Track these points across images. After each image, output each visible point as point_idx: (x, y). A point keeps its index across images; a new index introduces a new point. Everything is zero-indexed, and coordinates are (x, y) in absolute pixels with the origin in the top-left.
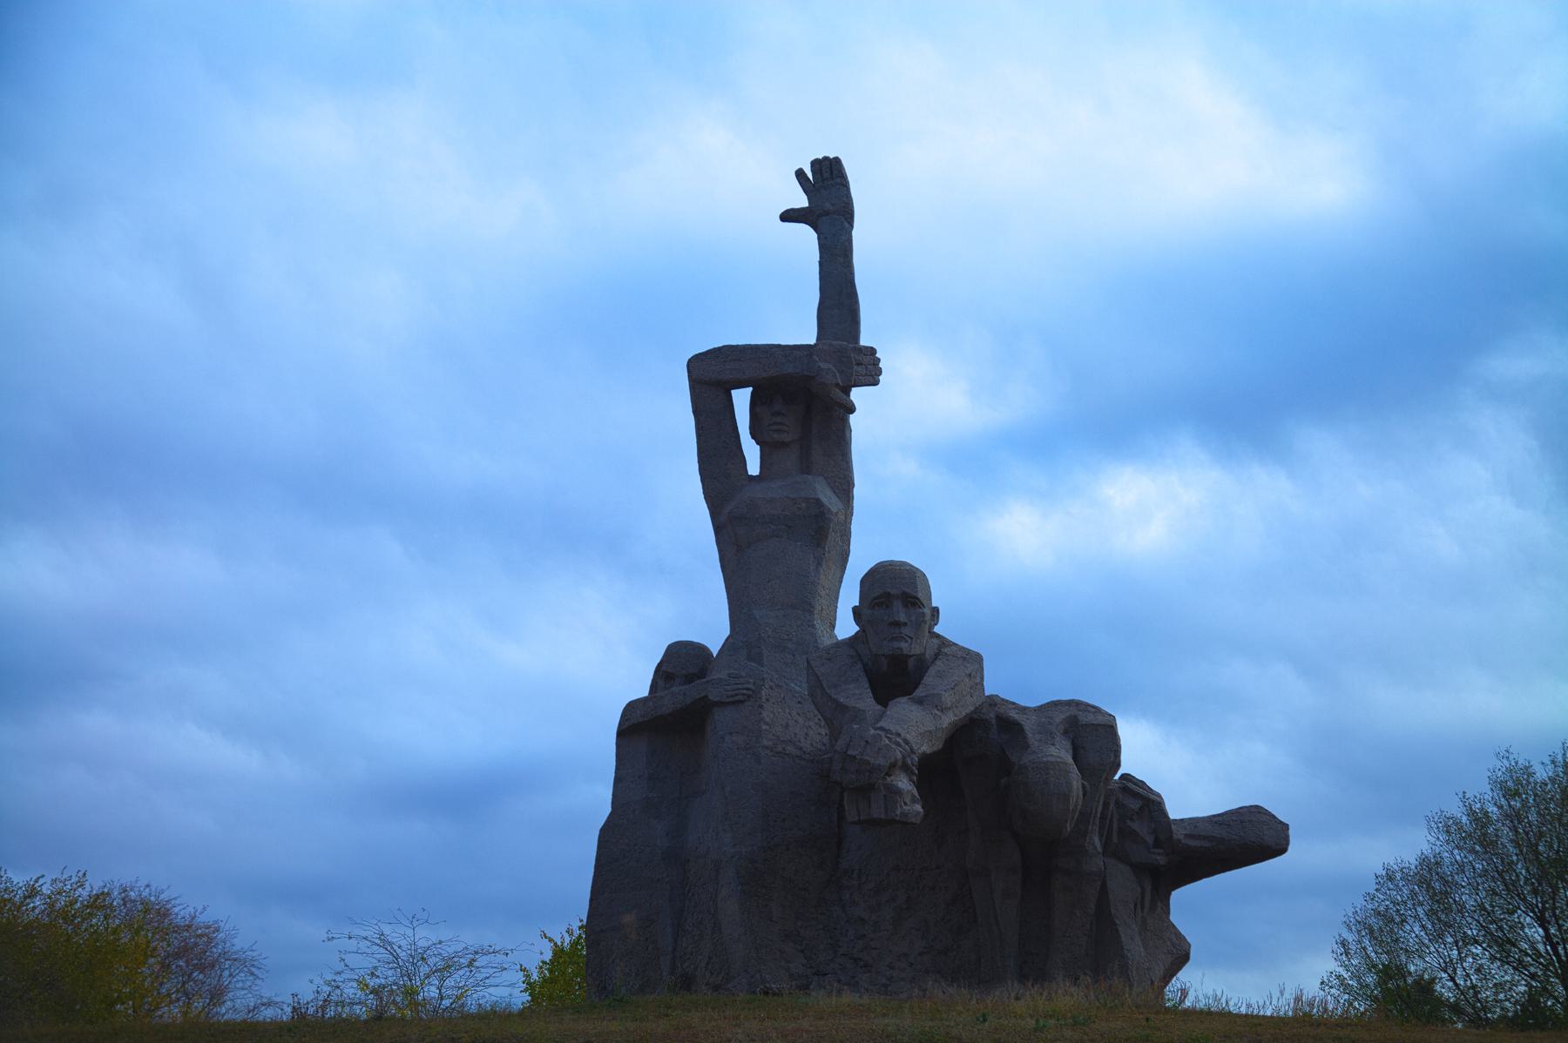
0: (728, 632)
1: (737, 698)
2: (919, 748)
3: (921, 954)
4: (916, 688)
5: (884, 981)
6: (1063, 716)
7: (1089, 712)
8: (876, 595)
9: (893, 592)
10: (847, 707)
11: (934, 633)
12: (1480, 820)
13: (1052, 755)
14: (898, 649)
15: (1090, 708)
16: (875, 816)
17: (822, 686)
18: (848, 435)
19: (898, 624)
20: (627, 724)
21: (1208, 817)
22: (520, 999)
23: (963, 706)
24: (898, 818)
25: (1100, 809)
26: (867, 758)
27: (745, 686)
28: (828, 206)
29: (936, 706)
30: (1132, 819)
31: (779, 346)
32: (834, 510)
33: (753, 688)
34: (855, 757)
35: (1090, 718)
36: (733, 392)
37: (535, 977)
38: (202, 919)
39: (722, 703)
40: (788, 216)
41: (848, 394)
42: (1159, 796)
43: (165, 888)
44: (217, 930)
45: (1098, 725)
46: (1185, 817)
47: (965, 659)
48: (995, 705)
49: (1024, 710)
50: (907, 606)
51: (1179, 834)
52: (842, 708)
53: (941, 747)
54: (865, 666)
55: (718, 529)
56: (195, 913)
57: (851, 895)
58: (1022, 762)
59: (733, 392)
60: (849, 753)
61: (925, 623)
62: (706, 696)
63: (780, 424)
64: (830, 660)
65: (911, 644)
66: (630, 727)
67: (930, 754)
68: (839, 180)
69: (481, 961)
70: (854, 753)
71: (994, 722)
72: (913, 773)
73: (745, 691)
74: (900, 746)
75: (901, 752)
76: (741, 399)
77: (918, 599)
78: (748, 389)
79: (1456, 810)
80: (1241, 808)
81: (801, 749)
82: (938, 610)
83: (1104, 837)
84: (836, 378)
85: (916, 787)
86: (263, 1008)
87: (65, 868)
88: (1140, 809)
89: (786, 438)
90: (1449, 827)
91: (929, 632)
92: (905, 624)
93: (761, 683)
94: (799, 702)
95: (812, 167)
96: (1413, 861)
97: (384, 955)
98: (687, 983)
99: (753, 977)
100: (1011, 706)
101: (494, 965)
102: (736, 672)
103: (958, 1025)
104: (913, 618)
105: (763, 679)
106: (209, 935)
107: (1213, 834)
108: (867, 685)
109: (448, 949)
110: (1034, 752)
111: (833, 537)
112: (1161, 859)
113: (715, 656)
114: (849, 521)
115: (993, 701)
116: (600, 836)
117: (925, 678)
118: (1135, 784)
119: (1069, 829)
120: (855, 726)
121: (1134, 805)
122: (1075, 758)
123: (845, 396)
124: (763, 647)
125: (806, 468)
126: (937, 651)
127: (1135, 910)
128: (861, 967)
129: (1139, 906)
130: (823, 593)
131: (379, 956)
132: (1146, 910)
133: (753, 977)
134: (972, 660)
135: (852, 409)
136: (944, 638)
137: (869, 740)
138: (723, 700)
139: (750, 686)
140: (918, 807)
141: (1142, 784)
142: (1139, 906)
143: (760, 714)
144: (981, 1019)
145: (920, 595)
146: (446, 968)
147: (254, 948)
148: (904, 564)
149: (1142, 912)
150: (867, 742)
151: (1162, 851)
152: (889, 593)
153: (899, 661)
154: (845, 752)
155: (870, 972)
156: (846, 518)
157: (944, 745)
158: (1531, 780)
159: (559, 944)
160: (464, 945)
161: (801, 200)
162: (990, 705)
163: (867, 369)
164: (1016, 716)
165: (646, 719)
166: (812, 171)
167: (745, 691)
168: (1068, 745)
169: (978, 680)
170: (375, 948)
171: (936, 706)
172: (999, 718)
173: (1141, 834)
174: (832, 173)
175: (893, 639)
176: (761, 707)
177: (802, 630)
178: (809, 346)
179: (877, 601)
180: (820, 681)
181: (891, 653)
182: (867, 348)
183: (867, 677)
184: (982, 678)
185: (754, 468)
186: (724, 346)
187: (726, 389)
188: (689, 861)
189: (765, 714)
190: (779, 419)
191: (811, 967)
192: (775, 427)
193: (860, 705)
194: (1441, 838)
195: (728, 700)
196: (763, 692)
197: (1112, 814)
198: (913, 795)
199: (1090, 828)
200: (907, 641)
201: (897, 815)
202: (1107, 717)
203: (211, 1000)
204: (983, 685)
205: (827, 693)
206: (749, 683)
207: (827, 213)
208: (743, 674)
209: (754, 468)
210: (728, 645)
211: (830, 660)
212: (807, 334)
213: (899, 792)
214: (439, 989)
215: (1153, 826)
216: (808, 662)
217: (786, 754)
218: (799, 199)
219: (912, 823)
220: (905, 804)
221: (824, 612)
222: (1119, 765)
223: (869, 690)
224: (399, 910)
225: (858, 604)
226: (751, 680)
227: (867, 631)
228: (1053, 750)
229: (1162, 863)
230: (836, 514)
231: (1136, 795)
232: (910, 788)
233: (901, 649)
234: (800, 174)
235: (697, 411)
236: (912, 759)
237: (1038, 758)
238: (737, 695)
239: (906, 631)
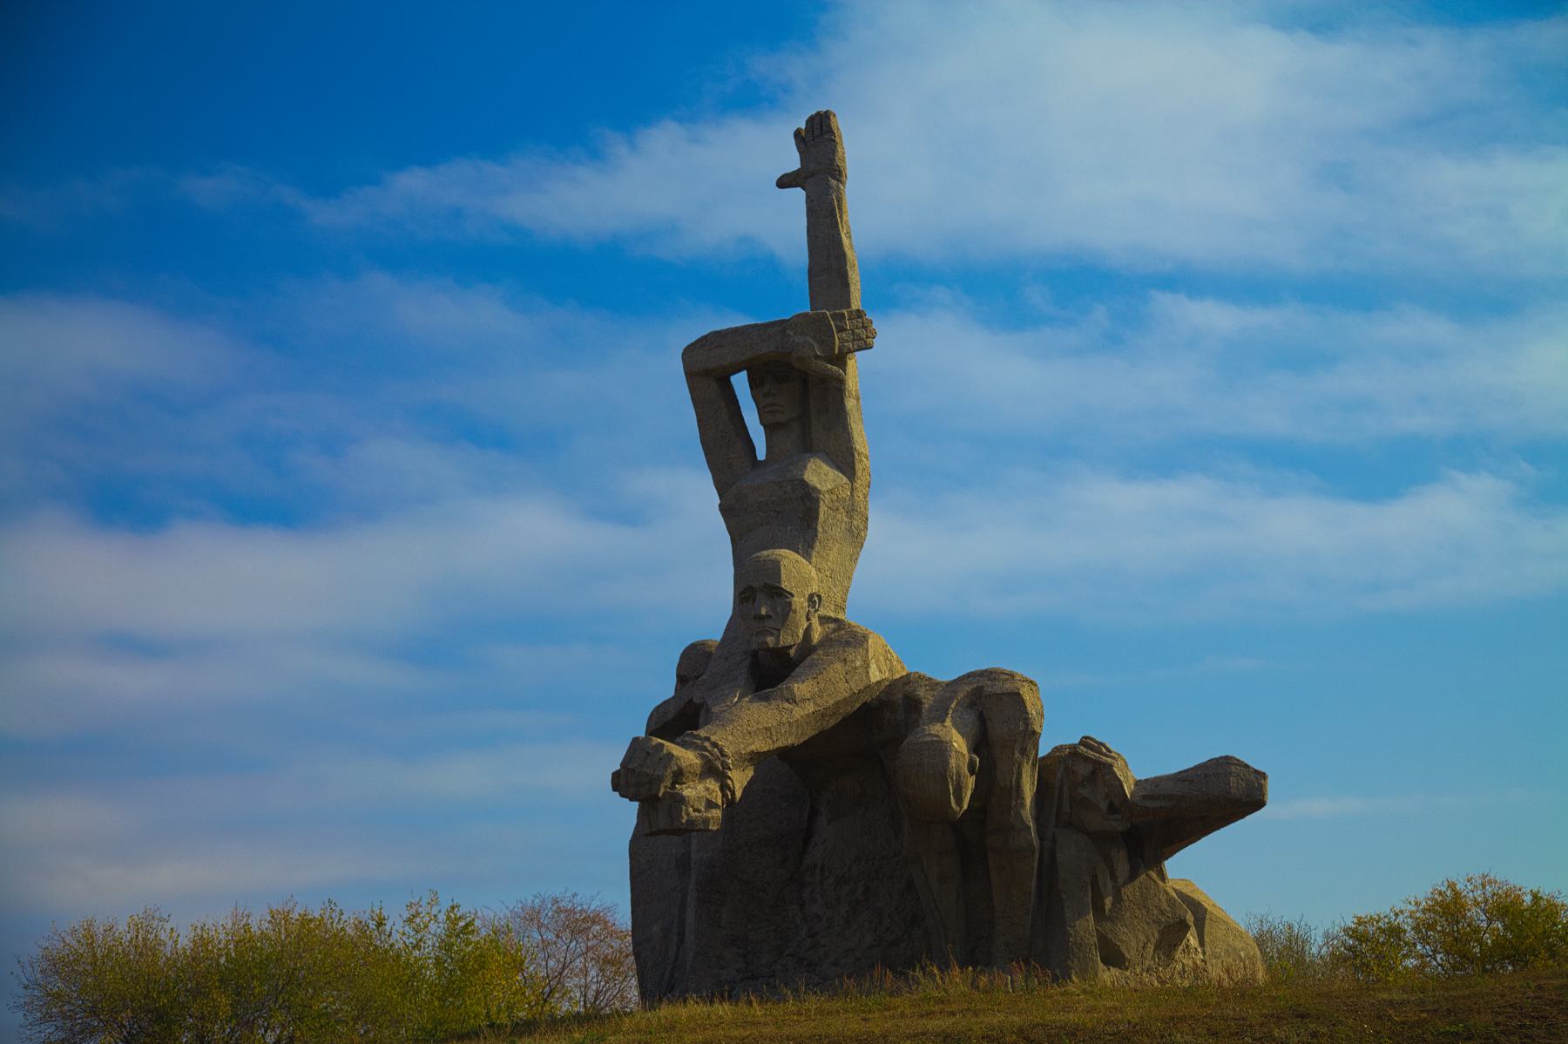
19: (760, 618)
40: (785, 182)
43: (436, 913)
45: (1003, 694)
50: (773, 597)
60: (629, 767)
63: (774, 405)
65: (779, 636)
76: (740, 382)
77: (782, 589)
78: (742, 373)
84: (814, 351)
87: (412, 893)
92: (768, 616)
96: (184, 942)
121: (1083, 770)
125: (808, 448)
137: (651, 751)
151: (1120, 817)
156: (852, 492)
190: (770, 400)
199: (1014, 803)
201: (683, 824)
209: (761, 454)
212: (801, 304)
218: (792, 162)
237: (916, 738)
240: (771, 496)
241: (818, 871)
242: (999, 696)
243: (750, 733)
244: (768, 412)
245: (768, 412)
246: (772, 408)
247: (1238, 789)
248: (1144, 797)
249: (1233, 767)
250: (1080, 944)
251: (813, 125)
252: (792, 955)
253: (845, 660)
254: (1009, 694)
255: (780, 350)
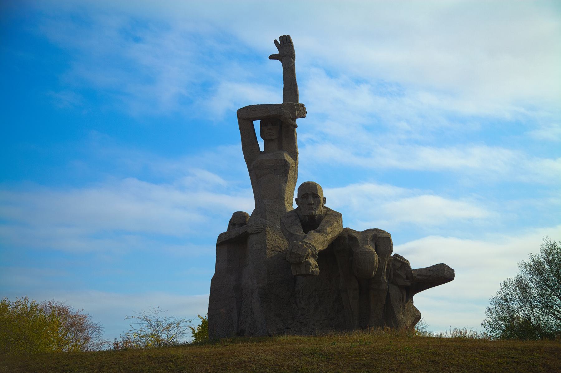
0: (254, 208)
1: (257, 232)
2: (318, 248)
3: (324, 320)
4: (318, 226)
5: (311, 330)
6: (371, 234)
7: (381, 233)
8: (303, 194)
9: (309, 193)
10: (294, 234)
11: (325, 206)
12: (537, 263)
13: (367, 249)
14: (311, 213)
15: (381, 231)
16: (302, 273)
17: (285, 227)
18: (295, 136)
19: (311, 204)
20: (220, 242)
21: (435, 265)
22: (189, 338)
23: (334, 233)
24: (310, 274)
25: (386, 267)
26: (298, 253)
27: (260, 227)
28: (286, 53)
29: (325, 233)
30: (398, 270)
31: (269, 105)
32: (291, 163)
33: (263, 228)
34: (294, 252)
35: (381, 235)
36: (253, 121)
37: (196, 331)
38: (81, 313)
39: (253, 233)
40: (272, 57)
41: (295, 121)
42: (408, 261)
44: (86, 317)
45: (384, 237)
46: (417, 268)
47: (335, 215)
48: (348, 231)
49: (358, 233)
50: (314, 198)
51: (415, 274)
52: (292, 235)
53: (327, 247)
54: (300, 219)
55: (250, 171)
56: (79, 311)
57: (299, 300)
58: (357, 252)
59: (253, 121)
60: (292, 251)
61: (321, 203)
62: (246, 231)
63: (271, 133)
64: (288, 217)
65: (316, 211)
66: (221, 243)
67: (323, 250)
68: (289, 43)
69: (182, 325)
70: (294, 251)
71: (347, 237)
72: (316, 257)
73: (260, 229)
74: (311, 248)
75: (311, 250)
77: (318, 195)
79: (529, 260)
80: (437, 264)
81: (281, 249)
82: (326, 199)
83: (388, 277)
85: (317, 262)
86: (104, 344)
88: (401, 266)
89: (273, 138)
90: (526, 266)
91: (323, 206)
92: (313, 204)
93: (266, 226)
94: (280, 232)
95: (280, 39)
97: (146, 324)
98: (241, 333)
99: (264, 330)
100: (353, 231)
101: (186, 326)
102: (257, 222)
103: (324, 346)
104: (316, 202)
105: (267, 224)
106: (83, 319)
107: (427, 274)
108: (301, 226)
109: (169, 321)
110: (361, 248)
111: (291, 173)
112: (409, 284)
113: (250, 216)
114: (297, 166)
115: (347, 230)
116: (211, 282)
117: (321, 223)
118: (399, 257)
119: (374, 274)
120: (294, 242)
121: (399, 265)
122: (376, 250)
123: (293, 122)
124: (266, 213)
125: (281, 148)
126: (326, 213)
127: (400, 302)
128: (303, 325)
129: (401, 301)
130: (288, 193)
131: (145, 324)
132: (404, 302)
133: (264, 330)
134: (338, 216)
135: (296, 127)
136: (328, 208)
138: (253, 232)
139: (262, 227)
140: (318, 269)
141: (402, 257)
142: (401, 301)
143: (266, 237)
144: (333, 344)
145: (319, 194)
146: (168, 328)
147: (100, 323)
148: (312, 183)
149: (403, 302)
150: (298, 247)
151: (409, 281)
152: (307, 193)
153: (312, 217)
154: (291, 251)
155: (306, 327)
156: (295, 165)
157: (328, 247)
158: (556, 248)
159: (205, 319)
160: (174, 319)
161: (276, 51)
162: (346, 231)
163: (301, 111)
164: (355, 235)
165: (226, 240)
166: (280, 40)
167: (260, 229)
168: (374, 245)
169: (340, 223)
170: (144, 321)
171: (325, 233)
172: (349, 236)
173: (401, 275)
174: (287, 41)
175: (309, 209)
176: (266, 234)
177: (280, 206)
178: (280, 104)
179: (303, 196)
180: (284, 225)
181: (309, 214)
182: (301, 104)
183: (301, 223)
184: (342, 222)
185: (262, 149)
186: (250, 106)
187: (251, 121)
188: (243, 290)
189: (267, 237)
191: (285, 326)
192: (269, 134)
193: (298, 234)
194: (523, 270)
195: (255, 232)
196: (267, 229)
197: (391, 268)
198: (316, 265)
200: (314, 210)
202: (388, 235)
203: (85, 341)
204: (342, 225)
205: (286, 229)
206: (262, 226)
207: (285, 56)
208: (259, 223)
210: (255, 212)
211: (288, 217)
213: (310, 264)
214: (167, 335)
215: (406, 272)
216: (280, 218)
217: (276, 251)
219: (315, 275)
220: (313, 268)
221: (288, 199)
222: (392, 251)
223: (302, 228)
224: (150, 306)
225: (297, 197)
226: (262, 225)
227: (300, 207)
228: (368, 247)
229: (409, 285)
230: (292, 165)
231: (399, 261)
232: (314, 263)
233: (312, 213)
234: (276, 42)
235: (241, 129)
236: (316, 252)
238: (257, 230)
239: (314, 206)
240: (273, 164)
241: (301, 293)
242: (383, 238)
243: (319, 243)
244: (268, 135)
245: (268, 135)
246: (271, 134)
247: (447, 274)
248: (418, 275)
249: (445, 267)
250: (401, 322)
251: (283, 39)
252: (297, 321)
253: (337, 221)
254: (386, 237)
255: (279, 114)
